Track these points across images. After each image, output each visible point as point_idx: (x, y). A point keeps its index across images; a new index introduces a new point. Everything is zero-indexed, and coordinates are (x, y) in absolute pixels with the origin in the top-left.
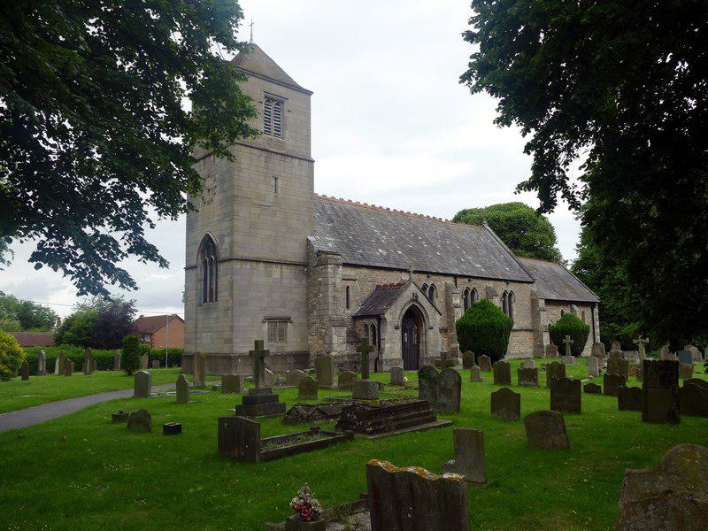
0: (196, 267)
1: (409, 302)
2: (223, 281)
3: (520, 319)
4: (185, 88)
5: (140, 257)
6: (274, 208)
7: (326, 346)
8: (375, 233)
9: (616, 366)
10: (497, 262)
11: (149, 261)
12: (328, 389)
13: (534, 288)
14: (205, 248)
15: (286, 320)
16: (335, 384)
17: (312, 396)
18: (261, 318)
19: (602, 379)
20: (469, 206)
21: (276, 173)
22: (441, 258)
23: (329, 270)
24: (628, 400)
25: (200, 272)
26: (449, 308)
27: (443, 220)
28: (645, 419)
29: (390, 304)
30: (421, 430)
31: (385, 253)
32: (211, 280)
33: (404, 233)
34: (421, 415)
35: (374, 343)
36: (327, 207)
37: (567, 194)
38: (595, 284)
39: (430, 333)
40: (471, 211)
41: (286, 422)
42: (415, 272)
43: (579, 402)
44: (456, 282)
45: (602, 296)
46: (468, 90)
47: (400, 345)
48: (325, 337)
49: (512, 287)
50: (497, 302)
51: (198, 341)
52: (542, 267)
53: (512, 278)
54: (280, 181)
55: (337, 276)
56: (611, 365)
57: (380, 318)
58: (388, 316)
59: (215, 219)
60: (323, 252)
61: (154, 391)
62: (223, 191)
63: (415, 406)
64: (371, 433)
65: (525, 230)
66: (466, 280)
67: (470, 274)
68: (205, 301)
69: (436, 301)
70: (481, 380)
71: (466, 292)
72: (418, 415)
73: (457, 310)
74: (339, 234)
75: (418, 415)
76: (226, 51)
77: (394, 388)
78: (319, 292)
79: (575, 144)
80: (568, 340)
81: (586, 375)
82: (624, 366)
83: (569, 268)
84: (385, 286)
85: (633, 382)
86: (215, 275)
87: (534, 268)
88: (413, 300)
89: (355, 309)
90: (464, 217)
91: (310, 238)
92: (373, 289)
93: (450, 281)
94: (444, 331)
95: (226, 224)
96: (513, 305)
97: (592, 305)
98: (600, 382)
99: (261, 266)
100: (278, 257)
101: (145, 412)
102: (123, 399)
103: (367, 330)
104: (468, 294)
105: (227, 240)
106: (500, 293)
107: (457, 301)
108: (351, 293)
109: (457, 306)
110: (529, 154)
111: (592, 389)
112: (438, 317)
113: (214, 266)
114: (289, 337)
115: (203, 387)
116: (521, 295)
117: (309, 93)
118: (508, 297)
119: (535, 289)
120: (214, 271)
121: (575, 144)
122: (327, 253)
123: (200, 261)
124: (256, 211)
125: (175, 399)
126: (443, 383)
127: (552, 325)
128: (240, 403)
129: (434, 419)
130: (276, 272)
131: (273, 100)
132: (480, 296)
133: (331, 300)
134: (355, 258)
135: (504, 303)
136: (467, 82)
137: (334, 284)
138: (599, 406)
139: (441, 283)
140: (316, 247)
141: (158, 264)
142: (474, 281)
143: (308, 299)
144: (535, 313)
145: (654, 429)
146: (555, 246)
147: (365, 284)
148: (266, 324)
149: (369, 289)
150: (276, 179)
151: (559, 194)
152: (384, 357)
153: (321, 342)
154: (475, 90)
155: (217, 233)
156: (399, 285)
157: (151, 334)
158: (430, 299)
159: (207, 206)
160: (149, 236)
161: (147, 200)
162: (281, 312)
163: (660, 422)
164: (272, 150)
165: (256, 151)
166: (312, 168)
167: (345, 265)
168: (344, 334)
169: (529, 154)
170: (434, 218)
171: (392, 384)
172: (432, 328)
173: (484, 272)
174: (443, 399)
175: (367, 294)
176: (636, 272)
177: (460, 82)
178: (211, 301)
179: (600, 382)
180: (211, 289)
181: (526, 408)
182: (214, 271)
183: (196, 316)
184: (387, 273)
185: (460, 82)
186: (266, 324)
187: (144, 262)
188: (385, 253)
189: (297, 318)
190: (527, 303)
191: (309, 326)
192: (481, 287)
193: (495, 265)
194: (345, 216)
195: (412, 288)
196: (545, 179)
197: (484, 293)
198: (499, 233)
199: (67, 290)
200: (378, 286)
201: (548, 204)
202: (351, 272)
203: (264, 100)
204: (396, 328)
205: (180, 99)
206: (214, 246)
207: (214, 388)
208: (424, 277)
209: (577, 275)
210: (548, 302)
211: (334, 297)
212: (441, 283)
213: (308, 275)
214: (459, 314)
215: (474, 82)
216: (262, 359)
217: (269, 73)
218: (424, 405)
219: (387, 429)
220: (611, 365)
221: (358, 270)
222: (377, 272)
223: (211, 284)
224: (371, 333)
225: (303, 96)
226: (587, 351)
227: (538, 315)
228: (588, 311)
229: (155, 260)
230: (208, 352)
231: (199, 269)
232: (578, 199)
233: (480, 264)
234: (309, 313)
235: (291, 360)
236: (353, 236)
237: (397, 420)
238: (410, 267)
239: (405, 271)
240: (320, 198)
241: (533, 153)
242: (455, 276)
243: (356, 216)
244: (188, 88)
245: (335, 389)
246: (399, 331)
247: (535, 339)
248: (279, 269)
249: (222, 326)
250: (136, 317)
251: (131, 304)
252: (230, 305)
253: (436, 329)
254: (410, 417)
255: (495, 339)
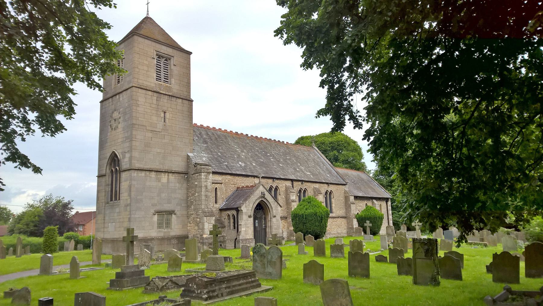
0: (105, 175)
1: (259, 198)
2: (124, 185)
3: (338, 209)
4: (65, 35)
5: (16, 164)
6: (163, 133)
7: (200, 231)
8: (236, 151)
9: (399, 242)
10: (321, 171)
11: (23, 168)
12: (194, 263)
13: (346, 188)
14: (112, 161)
15: (171, 213)
16: (199, 259)
17: (177, 269)
18: (153, 211)
19: (387, 252)
20: (305, 135)
21: (165, 109)
22: (282, 168)
23: (203, 177)
24: (405, 268)
25: (108, 179)
26: (288, 202)
27: (285, 143)
28: (415, 283)
29: (246, 200)
30: (247, 295)
31: (243, 165)
32: (116, 185)
33: (258, 151)
34: (249, 283)
35: (235, 228)
36: (203, 133)
37: (353, 118)
38: (389, 186)
39: (274, 220)
40: (307, 138)
41: (507, 228)
42: (263, 177)
43: (367, 269)
44: (293, 184)
45: (394, 194)
46: (281, 42)
47: (252, 228)
48: (199, 225)
49: (331, 188)
50: (321, 198)
51: (106, 230)
52: (352, 174)
53: (332, 182)
54: (167, 115)
55: (208, 181)
56: (396, 241)
57: (238, 210)
58: (243, 208)
59: (120, 140)
60: (198, 164)
61: (55, 270)
62: (125, 120)
63: (245, 276)
64: (206, 300)
65: (342, 150)
66: (300, 183)
67: (303, 179)
68: (111, 200)
69: (279, 197)
70: (305, 253)
71: (300, 191)
72: (247, 283)
73: (293, 204)
74: (212, 152)
75: (247, 283)
76: (93, 6)
77: (242, 260)
78: (195, 191)
79: (360, 83)
80: (368, 224)
81: (380, 248)
82: (404, 241)
83: (371, 175)
84: (243, 187)
85: (409, 254)
86: (118, 181)
87: (347, 175)
88: (262, 197)
89: (221, 204)
90: (302, 141)
91: (191, 155)
92: (235, 189)
93: (289, 184)
94: (283, 218)
95: (127, 144)
96: (333, 200)
97: (387, 200)
98: (386, 254)
99: (153, 174)
100: (166, 168)
101: (27, 289)
102: (30, 277)
103: (229, 219)
104: (302, 193)
105: (127, 155)
106: (323, 192)
107: (294, 197)
108: (218, 193)
109: (293, 201)
110: (323, 87)
111: (380, 259)
112: (279, 208)
113: (118, 175)
114: (173, 224)
115: (99, 264)
116: (338, 192)
117: (190, 53)
118: (328, 195)
119: (347, 189)
120: (118, 178)
121: (360, 83)
122: (201, 165)
123: (108, 171)
124: (150, 135)
125: (68, 276)
126: (269, 257)
127: (359, 213)
128: (114, 278)
129: (259, 285)
130: (164, 178)
131: (163, 57)
132: (310, 193)
133: (203, 198)
134: (222, 168)
135: (326, 198)
136: (280, 36)
137: (206, 187)
138: (384, 273)
139: (282, 185)
140: (194, 161)
141: (31, 169)
142: (305, 184)
143: (188, 197)
144: (347, 206)
145: (421, 290)
146: (363, 161)
147: (228, 186)
148: (156, 216)
149: (231, 190)
150: (165, 113)
151: (347, 117)
152: (241, 237)
153: (196, 228)
154: (287, 42)
155: (120, 151)
156: (252, 186)
157: (84, 225)
158: (275, 198)
159: (113, 132)
160: (21, 147)
161: (33, 121)
162: (167, 207)
163: (426, 284)
164: (162, 92)
165: (150, 93)
166: (192, 105)
167: (214, 173)
168: (213, 222)
169: (323, 87)
170: (279, 141)
171: (242, 257)
172: (275, 217)
173: (312, 178)
174: (270, 269)
175: (230, 193)
176: (404, 174)
177: (275, 36)
178: (116, 199)
179: (386, 254)
180: (116, 191)
181: (328, 275)
182: (118, 178)
183: (105, 211)
184: (245, 178)
185: (275, 36)
186: (156, 216)
187: (20, 168)
188: (243, 165)
189: (179, 211)
190: (342, 199)
191: (188, 217)
192: (310, 188)
193: (319, 173)
194: (216, 139)
195: (261, 189)
196: (337, 107)
197: (312, 192)
198: (324, 152)
199: (26, 195)
200: (238, 188)
201: (339, 125)
202: (218, 178)
203: (156, 57)
204: (250, 217)
205: (63, 44)
206: (119, 160)
207: (107, 265)
208: (270, 181)
209: (376, 180)
210: (356, 198)
211: (206, 196)
212: (282, 185)
213: (188, 180)
214: (294, 205)
215: (285, 36)
216: (132, 242)
217: (159, 38)
218: (252, 274)
219: (220, 295)
220: (396, 241)
221: (224, 177)
222: (237, 178)
223: (116, 187)
224: (232, 221)
225: (185, 55)
226: (383, 231)
227: (350, 207)
228: (384, 203)
229: (28, 167)
230: (112, 237)
231: (107, 177)
232: (360, 121)
233: (310, 172)
234: (188, 207)
235: (174, 242)
236: (221, 153)
237: (229, 287)
238: (260, 174)
239: (257, 177)
240: (198, 127)
241: (326, 87)
242: (292, 180)
243: (224, 140)
244: (67, 35)
245: (199, 263)
246: (252, 219)
247: (347, 223)
248: (166, 176)
249: (123, 218)
250: (73, 212)
251: (69, 203)
252: (129, 202)
253: (278, 217)
254: (240, 285)
255: (317, 224)
